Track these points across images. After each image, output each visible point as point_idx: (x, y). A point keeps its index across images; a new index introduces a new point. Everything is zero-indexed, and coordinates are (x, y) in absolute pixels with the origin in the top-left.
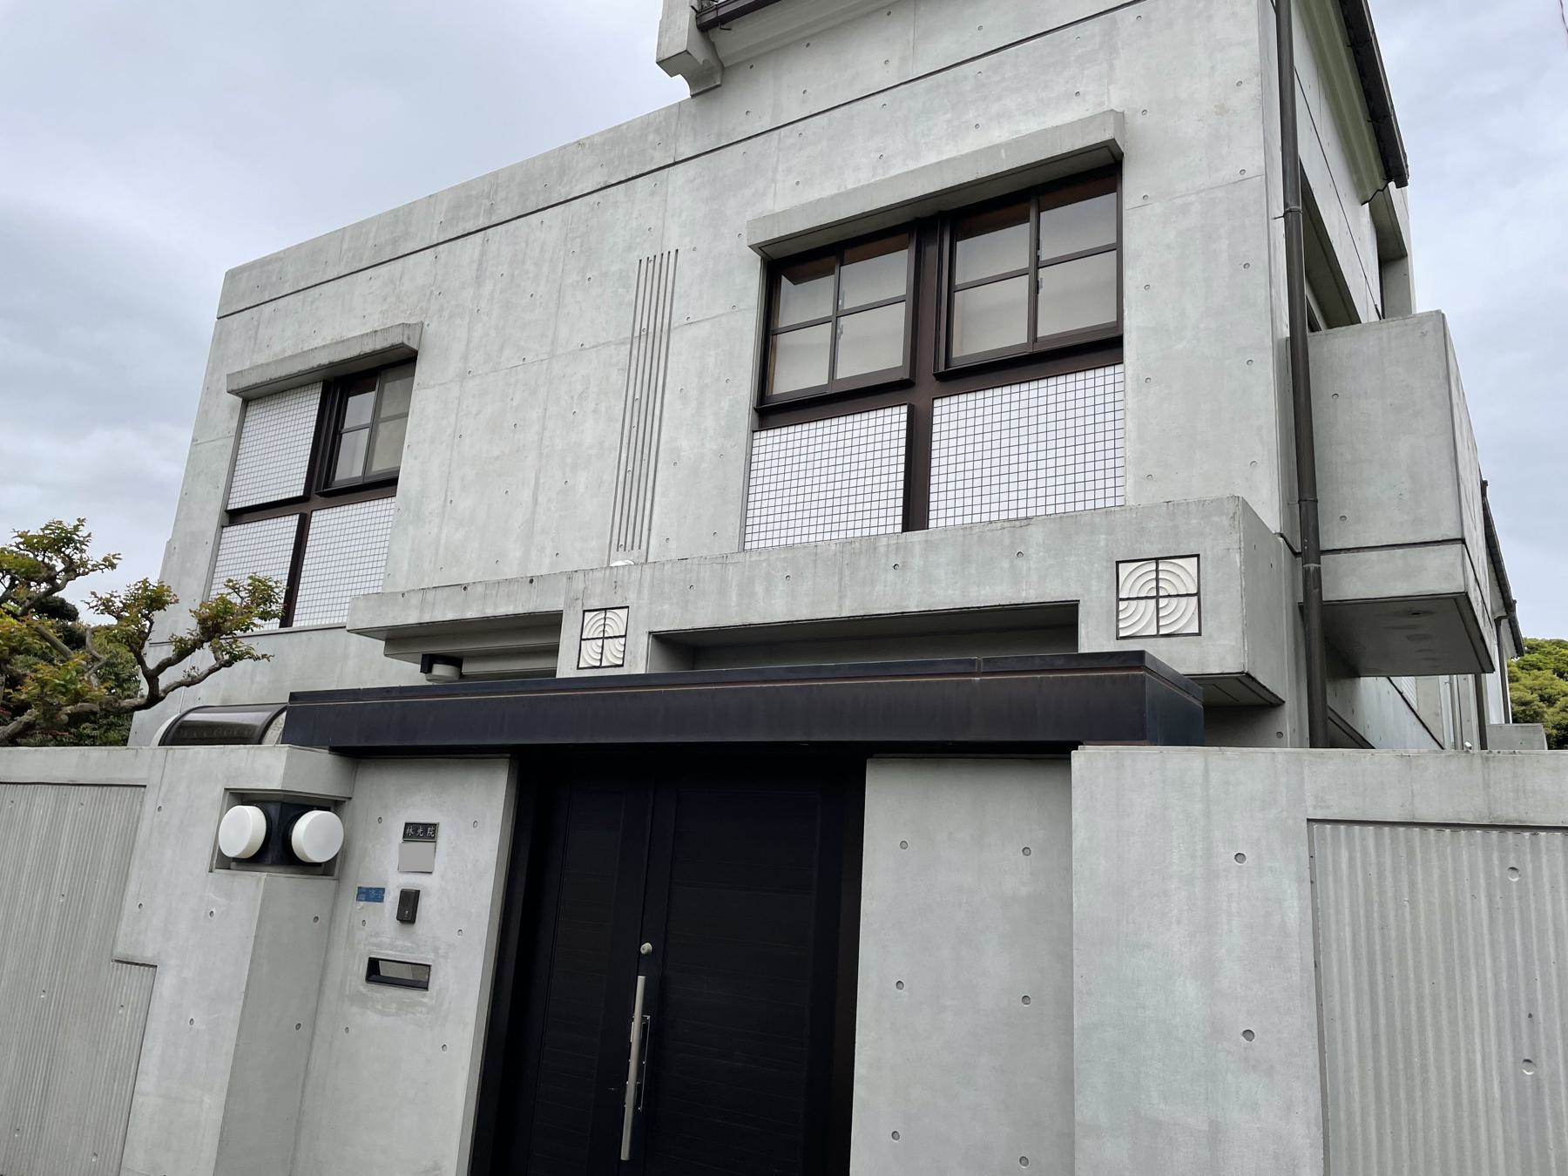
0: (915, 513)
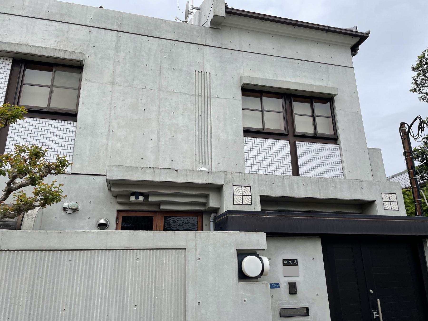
0: (296, 171)
